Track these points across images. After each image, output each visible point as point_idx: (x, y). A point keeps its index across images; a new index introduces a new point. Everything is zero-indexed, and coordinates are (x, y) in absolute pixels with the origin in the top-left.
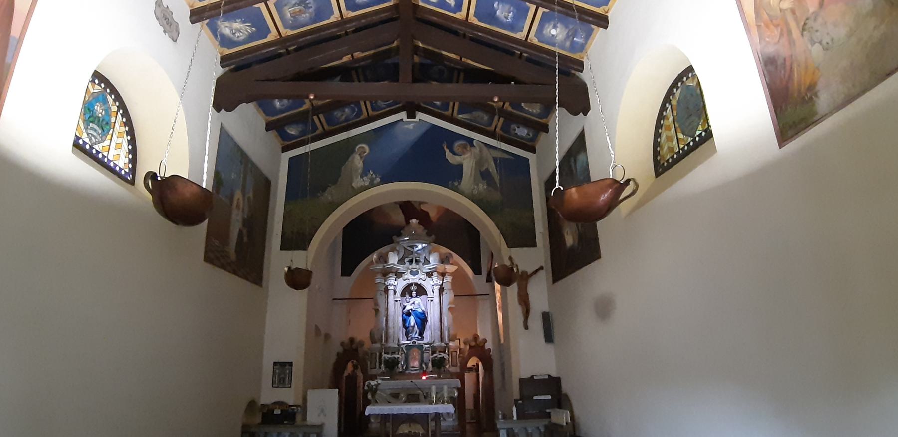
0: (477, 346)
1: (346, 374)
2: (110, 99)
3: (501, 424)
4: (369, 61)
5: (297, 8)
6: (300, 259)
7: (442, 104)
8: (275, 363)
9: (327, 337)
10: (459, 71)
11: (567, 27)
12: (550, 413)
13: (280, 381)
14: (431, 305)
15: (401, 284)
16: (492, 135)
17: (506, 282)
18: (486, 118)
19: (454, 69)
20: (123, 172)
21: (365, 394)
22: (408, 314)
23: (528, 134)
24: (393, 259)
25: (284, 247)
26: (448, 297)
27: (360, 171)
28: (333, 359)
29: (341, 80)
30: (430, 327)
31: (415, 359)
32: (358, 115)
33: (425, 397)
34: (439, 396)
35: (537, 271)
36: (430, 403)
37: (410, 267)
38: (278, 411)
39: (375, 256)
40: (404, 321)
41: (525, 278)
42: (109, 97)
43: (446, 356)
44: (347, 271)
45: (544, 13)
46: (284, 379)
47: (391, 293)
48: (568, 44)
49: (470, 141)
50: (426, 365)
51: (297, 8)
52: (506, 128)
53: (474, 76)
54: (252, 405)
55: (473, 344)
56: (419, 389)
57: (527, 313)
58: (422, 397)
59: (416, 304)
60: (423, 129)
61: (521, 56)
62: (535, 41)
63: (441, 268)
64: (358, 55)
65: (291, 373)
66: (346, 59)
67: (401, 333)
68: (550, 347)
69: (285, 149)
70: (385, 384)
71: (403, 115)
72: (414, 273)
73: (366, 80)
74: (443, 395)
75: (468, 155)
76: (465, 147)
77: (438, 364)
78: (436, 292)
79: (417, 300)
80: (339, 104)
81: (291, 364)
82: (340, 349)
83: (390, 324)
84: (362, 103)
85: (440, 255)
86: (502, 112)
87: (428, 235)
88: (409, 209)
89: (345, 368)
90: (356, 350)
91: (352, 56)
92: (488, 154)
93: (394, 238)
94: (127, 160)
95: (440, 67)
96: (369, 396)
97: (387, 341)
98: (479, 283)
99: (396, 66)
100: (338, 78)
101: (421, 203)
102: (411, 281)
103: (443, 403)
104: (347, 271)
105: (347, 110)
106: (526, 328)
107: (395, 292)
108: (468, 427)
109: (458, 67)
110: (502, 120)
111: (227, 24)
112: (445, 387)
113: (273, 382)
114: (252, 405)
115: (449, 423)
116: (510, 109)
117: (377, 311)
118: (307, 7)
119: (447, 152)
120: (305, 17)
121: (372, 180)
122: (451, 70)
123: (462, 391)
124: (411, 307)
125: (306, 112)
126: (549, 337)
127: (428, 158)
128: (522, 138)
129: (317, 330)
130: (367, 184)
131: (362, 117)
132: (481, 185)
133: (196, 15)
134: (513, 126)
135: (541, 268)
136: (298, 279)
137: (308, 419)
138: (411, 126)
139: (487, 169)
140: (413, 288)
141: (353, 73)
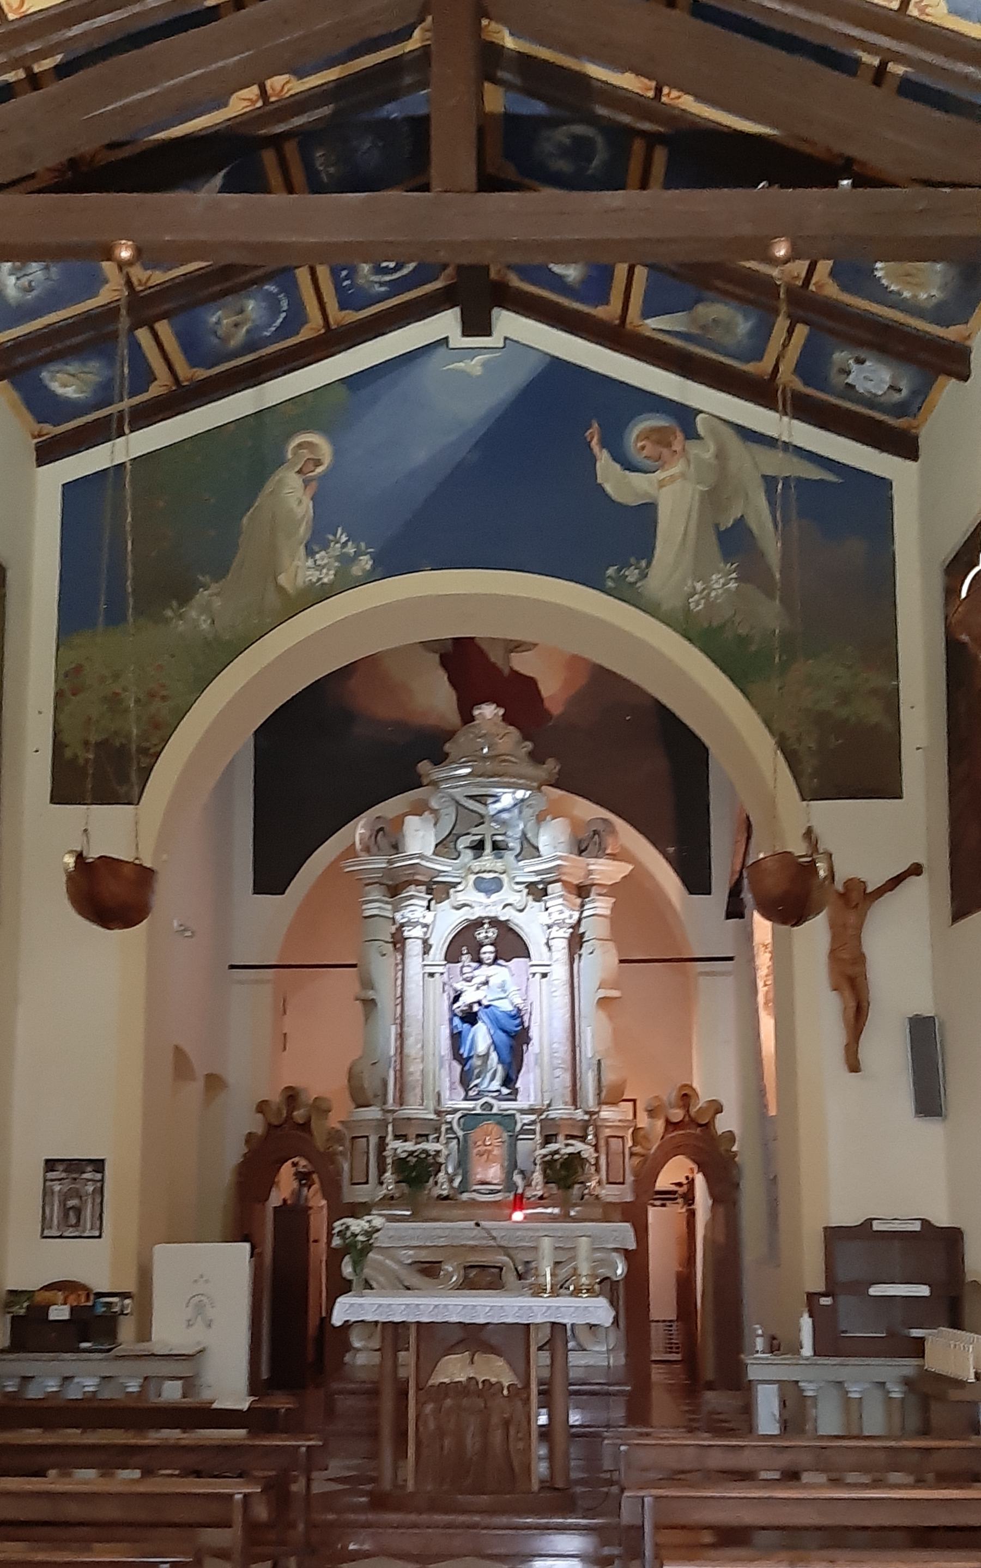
0: (690, 1122)
1: (275, 1199)
3: (761, 1367)
4: (326, 110)
6: (110, 831)
7: (587, 281)
8: (50, 1165)
9: (214, 1083)
10: (652, 140)
12: (921, 1340)
13: (66, 1211)
14: (542, 990)
15: (445, 921)
16: (761, 391)
17: (790, 908)
18: (743, 326)
19: (632, 132)
21: (335, 1256)
22: (470, 1018)
23: (894, 388)
24: (420, 838)
25: (63, 792)
26: (598, 961)
27: (303, 531)
29: (226, 188)
30: (538, 1056)
33: (520, 1277)
34: (564, 1272)
35: (896, 881)
36: (536, 1294)
37: (476, 865)
38: (59, 1313)
39: (359, 829)
40: (456, 1038)
41: (857, 899)
43: (587, 1151)
44: (272, 876)
46: (78, 1211)
47: (414, 948)
49: (684, 416)
52: (812, 365)
53: (708, 159)
55: (677, 1115)
56: (505, 1250)
57: (857, 1017)
58: (509, 1277)
59: (496, 984)
60: (520, 376)
61: (880, 75)
63: (577, 868)
64: (283, 85)
66: (242, 102)
67: (448, 1074)
68: (932, 1130)
69: (48, 452)
70: (394, 1233)
71: (446, 323)
72: (489, 886)
73: (316, 187)
74: (575, 1272)
75: (676, 469)
76: (661, 438)
77: (564, 1173)
78: (560, 946)
79: (499, 974)
80: (226, 280)
81: (99, 1165)
82: (257, 1125)
83: (412, 1047)
84: (303, 275)
85: (576, 825)
86: (804, 304)
88: (470, 666)
89: (271, 1183)
90: (305, 1126)
91: (263, 93)
92: (750, 465)
95: (580, 129)
96: (347, 1269)
97: (401, 1101)
98: (700, 919)
99: (419, 127)
100: (218, 180)
101: (517, 646)
102: (477, 913)
103: (577, 1293)
104: (272, 876)
105: (251, 305)
106: (854, 1066)
108: (657, 1374)
109: (647, 126)
110: (802, 331)
112: (584, 1243)
113: (45, 1222)
115: (597, 1357)
117: (369, 1004)
121: (346, 561)
122: (620, 137)
123: (637, 1259)
125: (110, 313)
126: (929, 1102)
127: (532, 483)
128: (871, 402)
129: (181, 1060)
131: (305, 334)
134: (841, 357)
135: (916, 870)
136: (109, 894)
139: (741, 521)
140: (486, 933)
141: (269, 157)
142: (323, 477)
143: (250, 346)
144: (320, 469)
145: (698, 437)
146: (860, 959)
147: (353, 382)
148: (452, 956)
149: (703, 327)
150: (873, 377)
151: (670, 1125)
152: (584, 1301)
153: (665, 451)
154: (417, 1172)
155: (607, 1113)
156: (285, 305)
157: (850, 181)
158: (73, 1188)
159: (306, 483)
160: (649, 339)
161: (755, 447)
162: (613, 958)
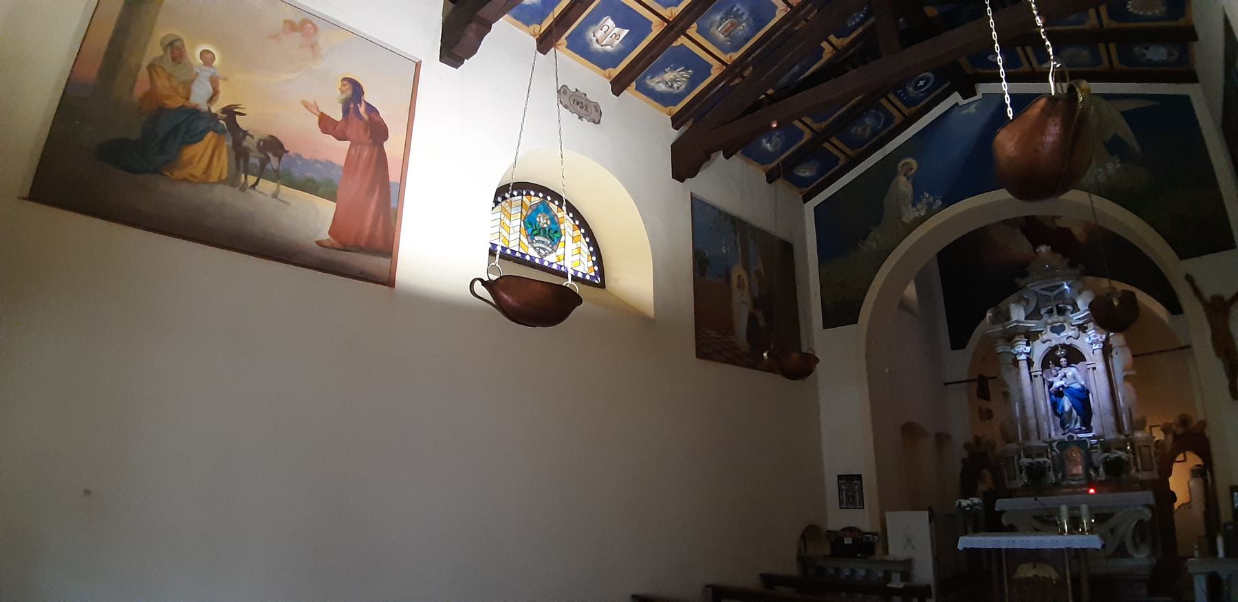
2: (554, 207)
5: (727, 23)
8: (840, 477)
13: (848, 498)
20: (588, 277)
23: (1170, 54)
24: (1018, 314)
25: (827, 324)
26: (1120, 360)
28: (958, 467)
31: (1076, 465)
32: (886, 124)
37: (1050, 321)
38: (848, 541)
40: (1055, 405)
42: (551, 205)
44: (959, 341)
46: (853, 498)
47: (1023, 365)
50: (1096, 469)
51: (727, 23)
54: (811, 533)
55: (1180, 431)
59: (1069, 376)
65: (861, 488)
69: (806, 198)
71: (956, 98)
72: (1057, 330)
77: (1116, 468)
78: (1099, 353)
79: (1071, 371)
80: (854, 115)
81: (859, 477)
82: (965, 454)
87: (1072, 264)
88: (1033, 229)
93: (1019, 281)
94: (591, 264)
102: (1054, 343)
104: (959, 341)
105: (867, 120)
107: (1030, 363)
111: (657, 79)
113: (841, 502)
114: (811, 533)
116: (1114, 24)
118: (737, 16)
120: (742, 28)
121: (930, 205)
124: (1062, 383)
128: (1164, 63)
132: (1110, 166)
133: (618, 86)
137: (891, 551)
138: (972, 109)
146: (1229, 337)
148: (1045, 365)
150: (1157, 53)
151: (1176, 436)
152: (1087, 537)
154: (1036, 473)
155: (1139, 435)
158: (850, 486)
162: (1128, 354)
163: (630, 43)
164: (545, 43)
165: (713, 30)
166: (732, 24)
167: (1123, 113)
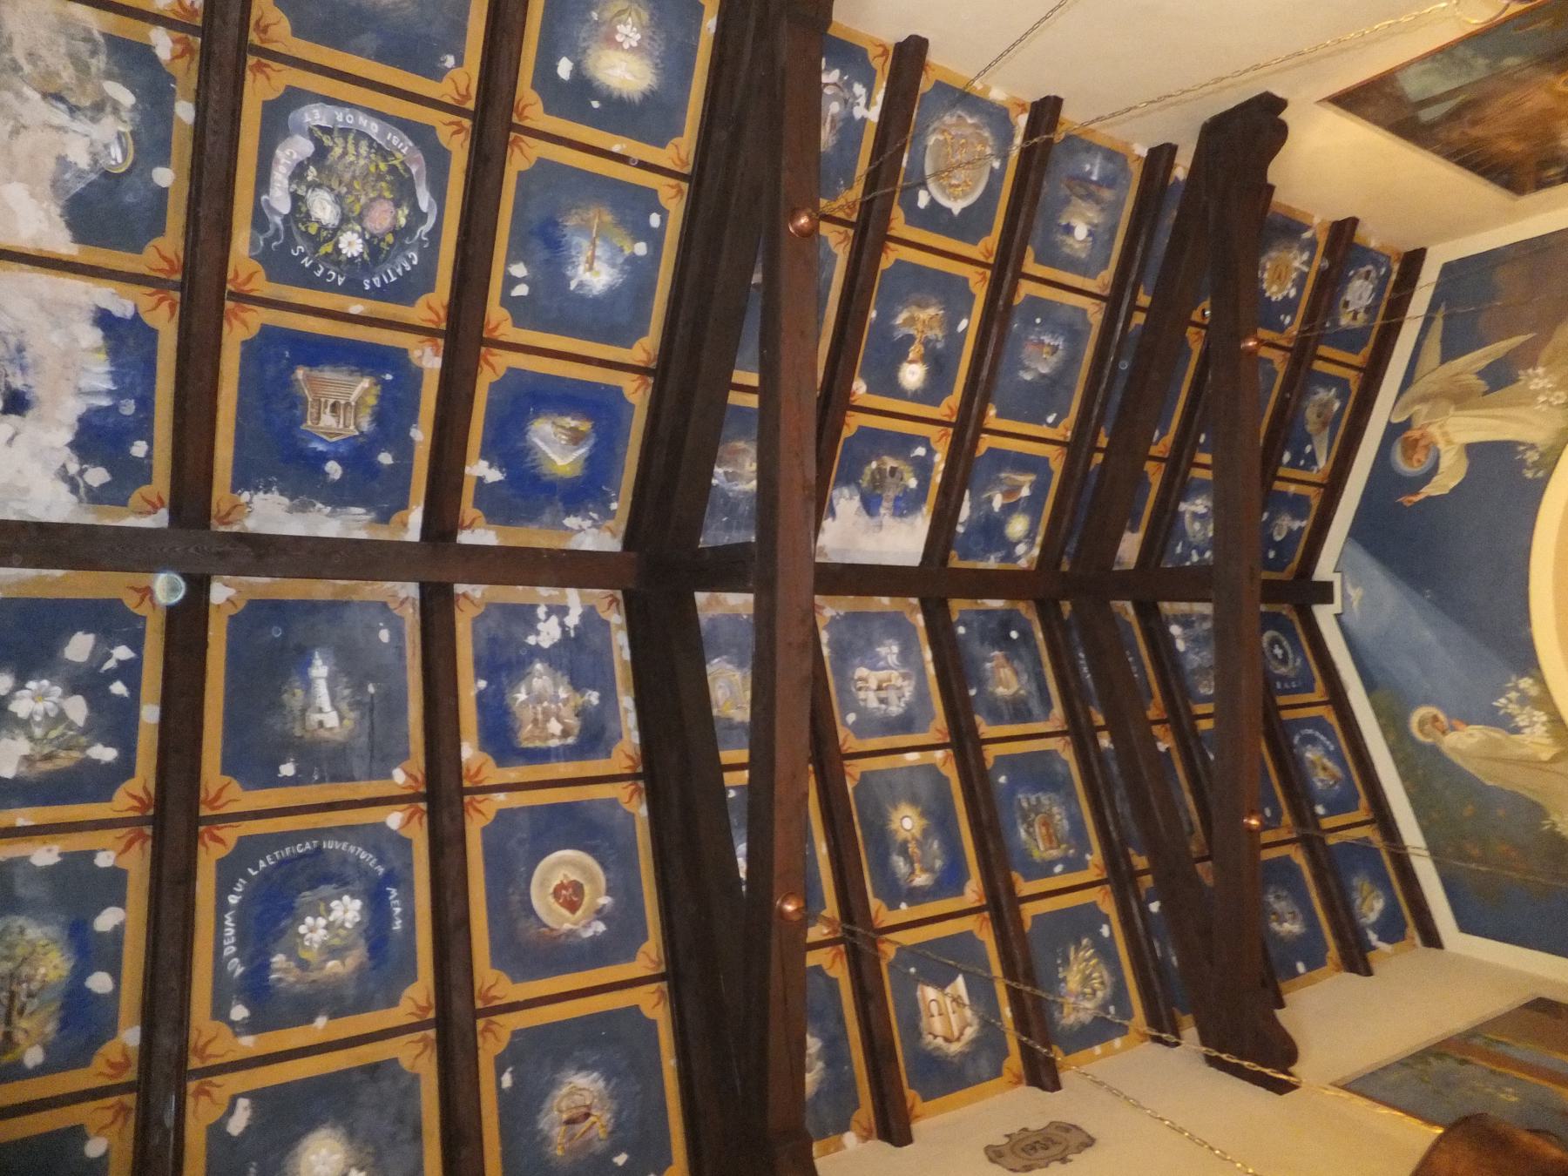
5: (1039, 830)
11: (1067, 201)
23: (1367, 276)
27: (1497, 734)
45: (1038, 260)
48: (1107, 194)
49: (1394, 432)
51: (1039, 830)
52: (1350, 339)
62: (1107, 276)
69: (1431, 938)
71: (1324, 615)
75: (1434, 430)
76: (1411, 447)
118: (1036, 809)
119: (1430, 490)
121: (1525, 699)
130: (1541, 717)
132: (1535, 385)
133: (1042, 1075)
134: (1345, 321)
139: (1481, 374)
142: (1449, 717)
143: (1342, 763)
144: (1442, 717)
145: (1410, 419)
147: (1370, 685)
149: (1324, 425)
150: (1359, 292)
153: (1422, 443)
156: (1310, 731)
157: (705, 541)
159: (1453, 729)
160: (1335, 463)
161: (1417, 375)
163: (981, 991)
164: (893, 1128)
165: (1036, 855)
166: (1045, 824)
167: (1443, 362)
